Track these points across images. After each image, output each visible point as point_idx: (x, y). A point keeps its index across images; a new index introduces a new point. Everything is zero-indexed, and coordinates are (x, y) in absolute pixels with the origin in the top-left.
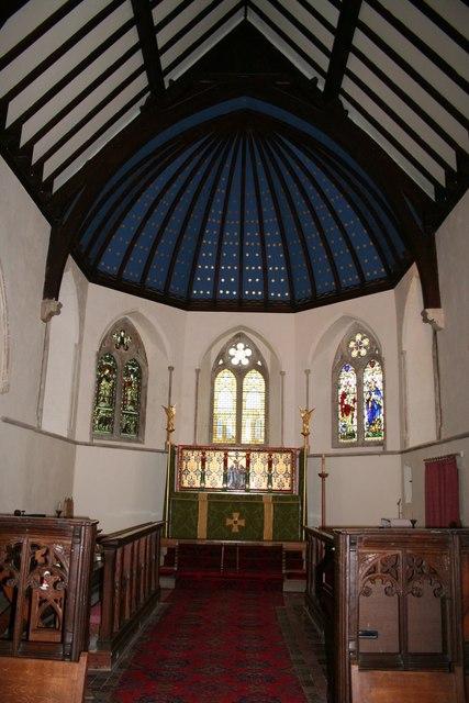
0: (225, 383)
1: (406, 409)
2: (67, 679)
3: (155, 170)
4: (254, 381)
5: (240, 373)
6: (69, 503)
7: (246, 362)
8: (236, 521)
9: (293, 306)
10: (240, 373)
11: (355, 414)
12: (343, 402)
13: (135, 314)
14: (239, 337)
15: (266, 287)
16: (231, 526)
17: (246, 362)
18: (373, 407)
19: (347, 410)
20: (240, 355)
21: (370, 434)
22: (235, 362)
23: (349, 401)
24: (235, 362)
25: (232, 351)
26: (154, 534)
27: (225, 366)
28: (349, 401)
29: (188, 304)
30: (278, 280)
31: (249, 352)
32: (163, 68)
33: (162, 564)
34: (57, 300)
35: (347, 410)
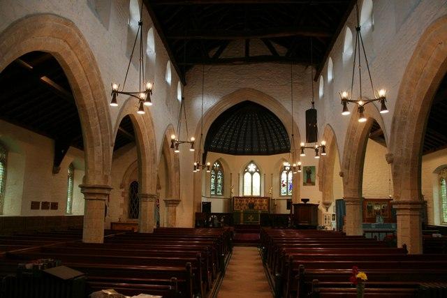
0: (247, 175)
2: (11, 208)
4: (257, 176)
5: (252, 173)
6: (77, 169)
8: (251, 218)
9: (268, 153)
10: (252, 173)
14: (252, 162)
17: (254, 170)
19: (284, 185)
20: (252, 167)
22: (250, 170)
23: (284, 183)
24: (250, 170)
25: (249, 167)
26: (219, 147)
28: (284, 183)
29: (236, 153)
31: (255, 167)
32: (271, 54)
34: (306, 69)
35: (284, 185)
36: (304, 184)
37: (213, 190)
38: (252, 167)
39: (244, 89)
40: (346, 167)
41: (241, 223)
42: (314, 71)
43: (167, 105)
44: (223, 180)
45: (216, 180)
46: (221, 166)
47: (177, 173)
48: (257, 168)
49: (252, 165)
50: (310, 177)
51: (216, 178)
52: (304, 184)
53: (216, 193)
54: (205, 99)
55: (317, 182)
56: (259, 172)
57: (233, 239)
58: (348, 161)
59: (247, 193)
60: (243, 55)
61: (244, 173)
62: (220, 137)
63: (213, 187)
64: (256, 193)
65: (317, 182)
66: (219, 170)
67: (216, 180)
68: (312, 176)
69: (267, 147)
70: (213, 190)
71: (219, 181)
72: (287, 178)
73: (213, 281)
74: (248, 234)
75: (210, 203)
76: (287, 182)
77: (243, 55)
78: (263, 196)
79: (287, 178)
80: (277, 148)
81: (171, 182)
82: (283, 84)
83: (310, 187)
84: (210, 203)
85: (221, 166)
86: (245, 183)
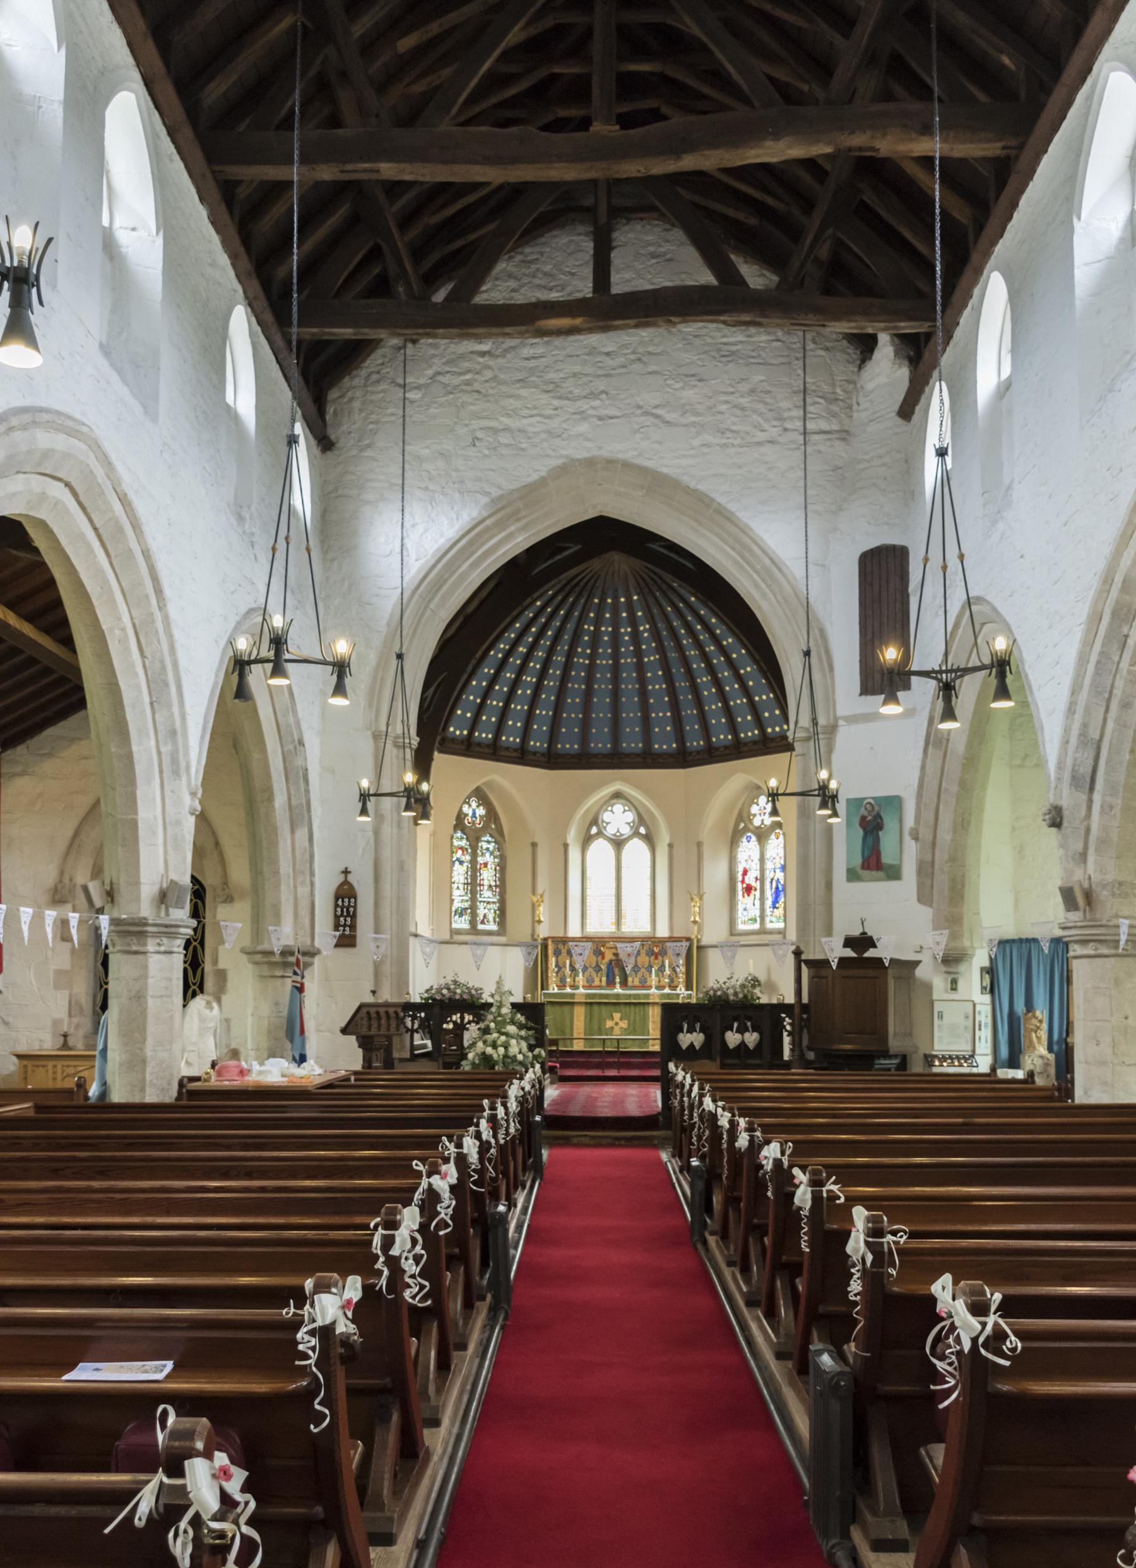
1: (370, 705)
3: (31, 706)
5: (618, 843)
7: (626, 831)
10: (618, 843)
11: (758, 893)
12: (743, 882)
13: (756, 889)
15: (733, 727)
16: (612, 1018)
17: (626, 831)
18: (777, 888)
19: (748, 889)
21: (774, 919)
22: (610, 831)
23: (750, 879)
24: (610, 831)
25: (606, 816)
27: (600, 834)
28: (750, 879)
30: (578, 674)
31: (630, 816)
33: (775, 1340)
35: (748, 889)
36: (852, 876)
37: (461, 913)
38: (618, 819)
39: (590, 463)
40: (1075, 780)
41: (578, 1046)
42: (903, 373)
43: (240, 519)
44: (502, 868)
45: (474, 870)
46: (492, 815)
47: (302, 834)
48: (641, 820)
49: (618, 808)
50: (877, 840)
51: (473, 861)
52: (852, 876)
53: (473, 923)
54: (416, 511)
55: (909, 870)
56: (649, 839)
57: (545, 1118)
58: (1090, 754)
59: (600, 923)
60: (584, 287)
61: (586, 841)
62: (487, 693)
63: (460, 898)
64: (637, 923)
65: (909, 870)
66: (485, 829)
67: (474, 870)
68: (888, 840)
69: (680, 734)
70: (461, 913)
71: (488, 876)
72: (762, 860)
73: (468, 1305)
74: (609, 1091)
75: (848, 800)
76: (761, 879)
77: (584, 287)
78: (663, 932)
79: (762, 860)
80: (696, 743)
81: (277, 872)
82: (762, 436)
83: (875, 890)
84: (848, 800)
85: (492, 815)
86: (589, 885)
